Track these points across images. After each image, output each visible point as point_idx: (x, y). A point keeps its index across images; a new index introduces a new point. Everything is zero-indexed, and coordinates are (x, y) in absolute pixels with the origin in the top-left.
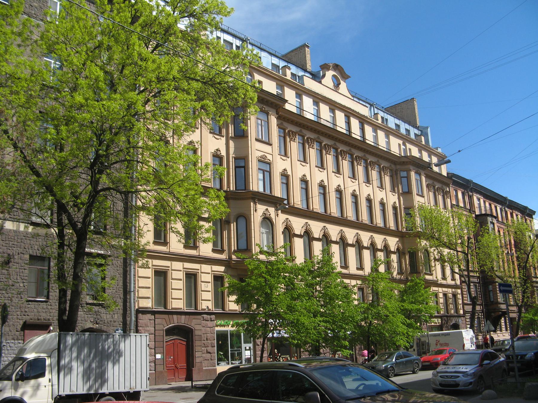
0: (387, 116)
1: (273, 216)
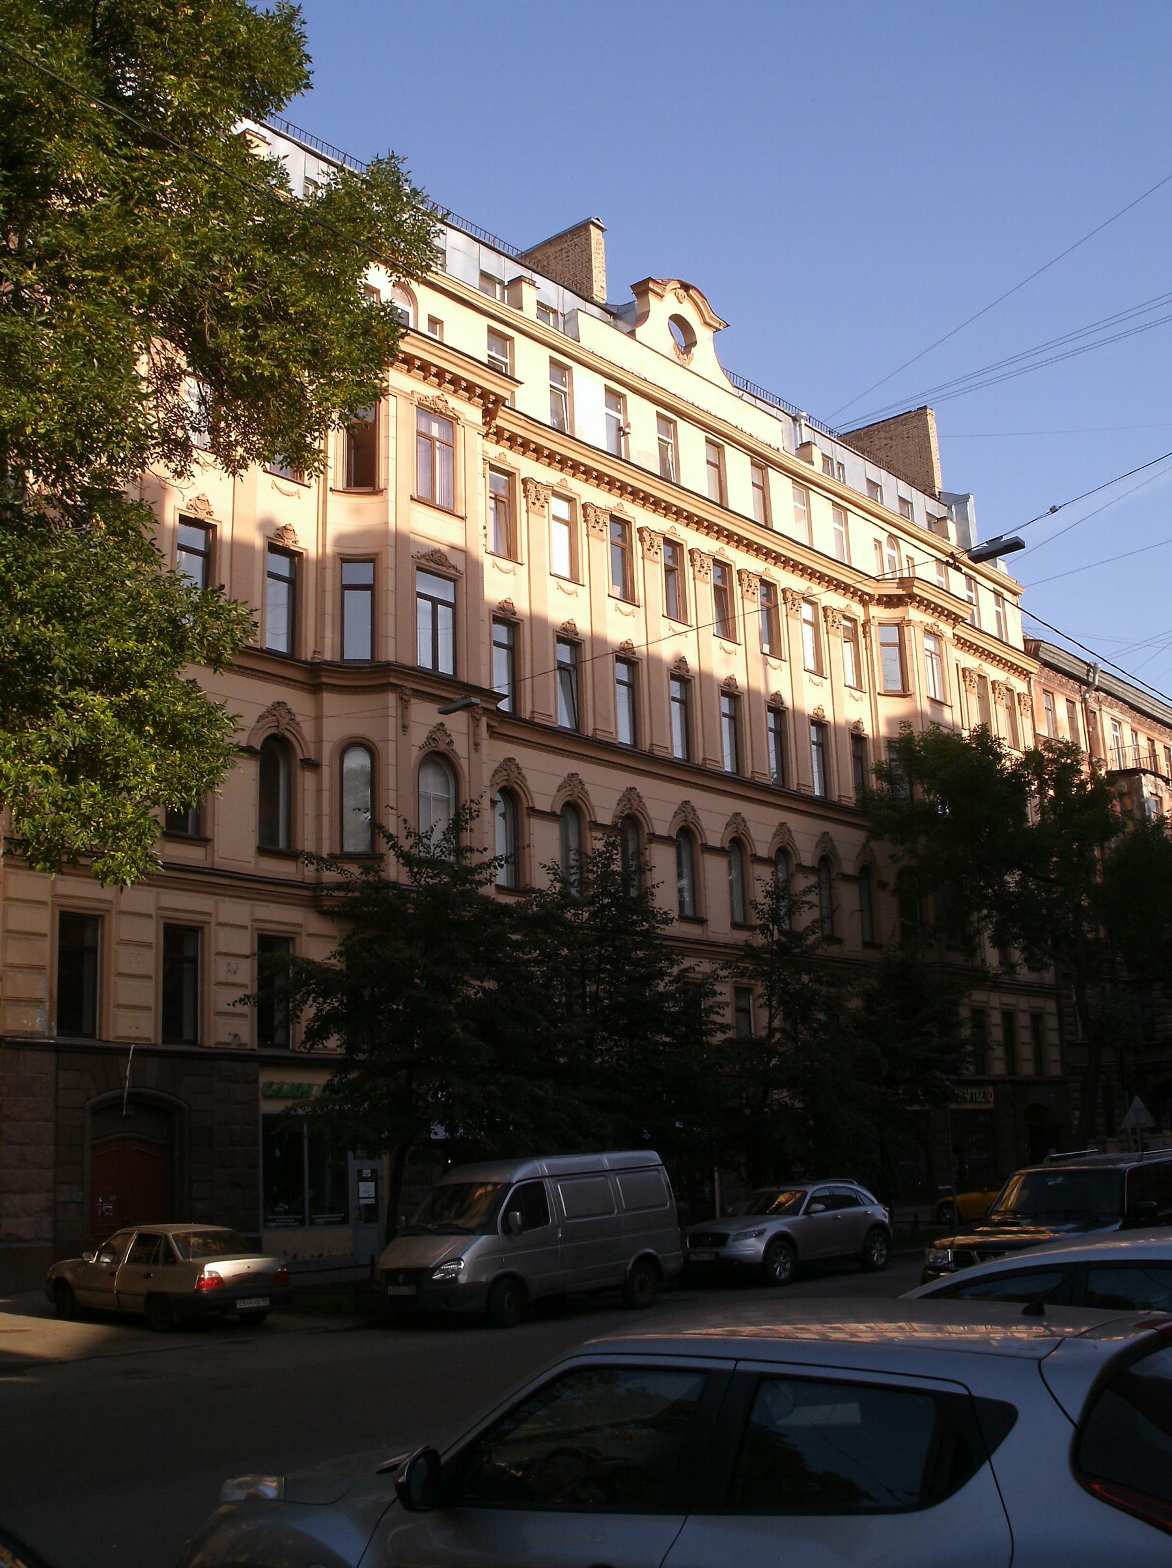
0: (842, 454)
1: (461, 747)
